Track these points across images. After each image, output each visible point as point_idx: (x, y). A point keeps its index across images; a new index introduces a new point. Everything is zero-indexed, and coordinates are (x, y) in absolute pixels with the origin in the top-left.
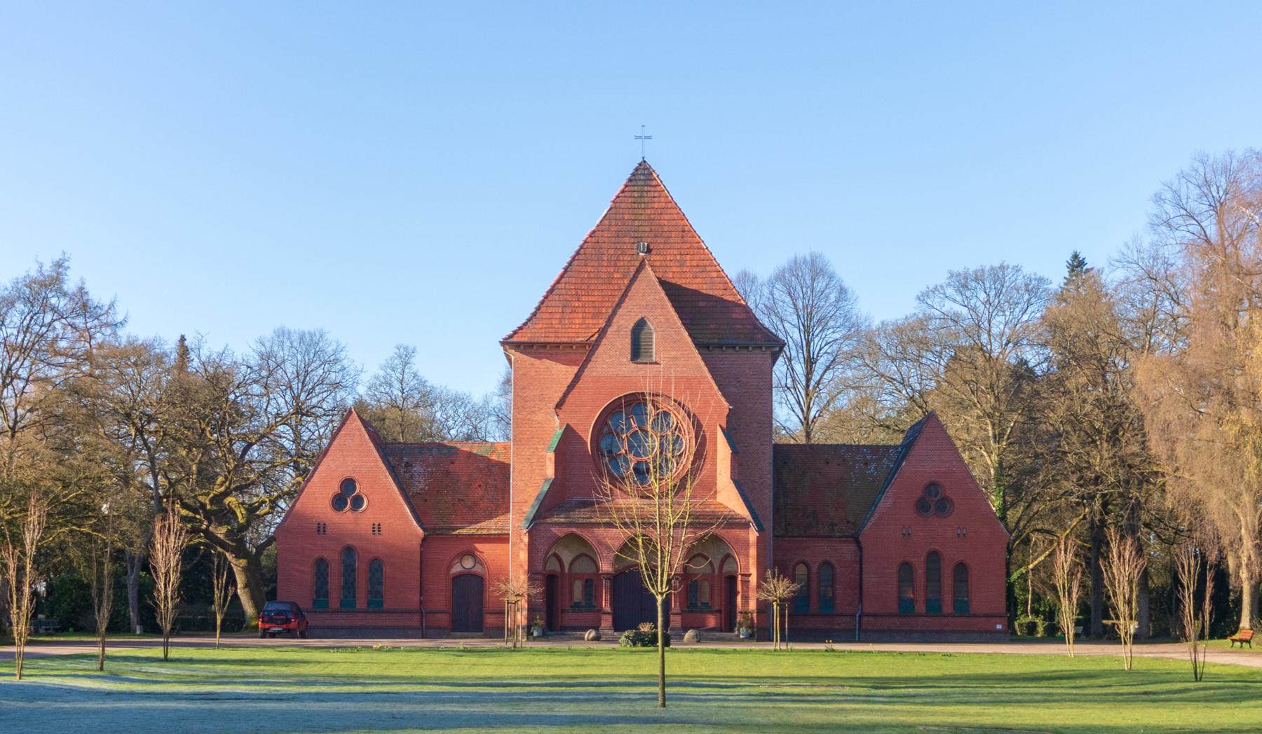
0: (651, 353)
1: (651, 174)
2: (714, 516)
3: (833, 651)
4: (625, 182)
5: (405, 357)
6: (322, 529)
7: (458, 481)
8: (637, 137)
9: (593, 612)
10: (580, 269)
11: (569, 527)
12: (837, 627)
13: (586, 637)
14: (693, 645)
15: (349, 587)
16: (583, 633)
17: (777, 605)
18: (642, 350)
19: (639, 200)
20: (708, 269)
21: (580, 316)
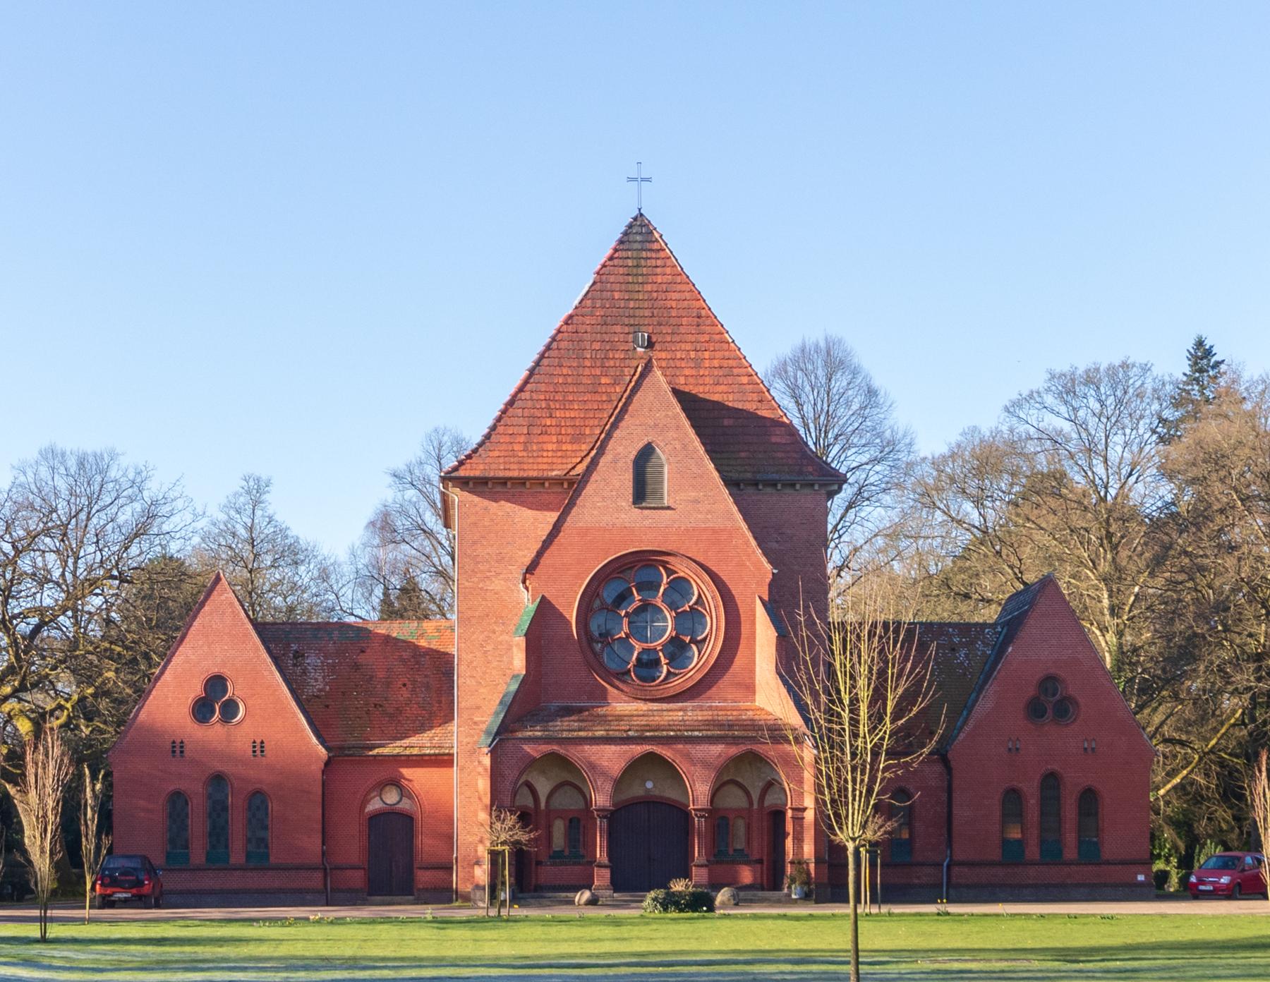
0: (662, 494)
1: (652, 232)
2: (754, 726)
3: (948, 914)
4: (613, 244)
5: (256, 491)
6: (178, 750)
7: (371, 677)
8: (631, 179)
9: (579, 864)
10: (551, 370)
11: (548, 743)
12: (916, 881)
13: (577, 899)
14: (731, 909)
15: (218, 834)
16: (570, 895)
17: (867, 851)
18: (649, 488)
19: (635, 271)
20: (736, 371)
21: (554, 439)
